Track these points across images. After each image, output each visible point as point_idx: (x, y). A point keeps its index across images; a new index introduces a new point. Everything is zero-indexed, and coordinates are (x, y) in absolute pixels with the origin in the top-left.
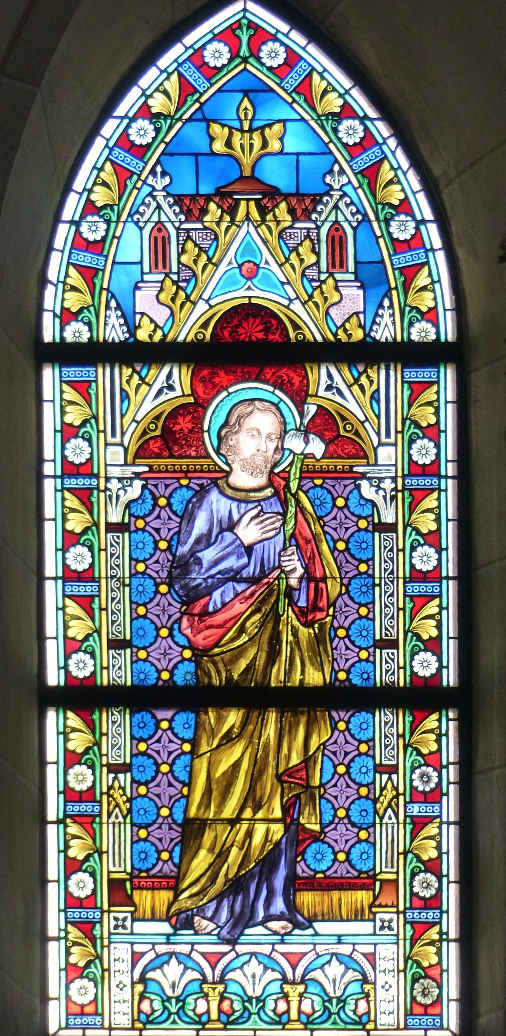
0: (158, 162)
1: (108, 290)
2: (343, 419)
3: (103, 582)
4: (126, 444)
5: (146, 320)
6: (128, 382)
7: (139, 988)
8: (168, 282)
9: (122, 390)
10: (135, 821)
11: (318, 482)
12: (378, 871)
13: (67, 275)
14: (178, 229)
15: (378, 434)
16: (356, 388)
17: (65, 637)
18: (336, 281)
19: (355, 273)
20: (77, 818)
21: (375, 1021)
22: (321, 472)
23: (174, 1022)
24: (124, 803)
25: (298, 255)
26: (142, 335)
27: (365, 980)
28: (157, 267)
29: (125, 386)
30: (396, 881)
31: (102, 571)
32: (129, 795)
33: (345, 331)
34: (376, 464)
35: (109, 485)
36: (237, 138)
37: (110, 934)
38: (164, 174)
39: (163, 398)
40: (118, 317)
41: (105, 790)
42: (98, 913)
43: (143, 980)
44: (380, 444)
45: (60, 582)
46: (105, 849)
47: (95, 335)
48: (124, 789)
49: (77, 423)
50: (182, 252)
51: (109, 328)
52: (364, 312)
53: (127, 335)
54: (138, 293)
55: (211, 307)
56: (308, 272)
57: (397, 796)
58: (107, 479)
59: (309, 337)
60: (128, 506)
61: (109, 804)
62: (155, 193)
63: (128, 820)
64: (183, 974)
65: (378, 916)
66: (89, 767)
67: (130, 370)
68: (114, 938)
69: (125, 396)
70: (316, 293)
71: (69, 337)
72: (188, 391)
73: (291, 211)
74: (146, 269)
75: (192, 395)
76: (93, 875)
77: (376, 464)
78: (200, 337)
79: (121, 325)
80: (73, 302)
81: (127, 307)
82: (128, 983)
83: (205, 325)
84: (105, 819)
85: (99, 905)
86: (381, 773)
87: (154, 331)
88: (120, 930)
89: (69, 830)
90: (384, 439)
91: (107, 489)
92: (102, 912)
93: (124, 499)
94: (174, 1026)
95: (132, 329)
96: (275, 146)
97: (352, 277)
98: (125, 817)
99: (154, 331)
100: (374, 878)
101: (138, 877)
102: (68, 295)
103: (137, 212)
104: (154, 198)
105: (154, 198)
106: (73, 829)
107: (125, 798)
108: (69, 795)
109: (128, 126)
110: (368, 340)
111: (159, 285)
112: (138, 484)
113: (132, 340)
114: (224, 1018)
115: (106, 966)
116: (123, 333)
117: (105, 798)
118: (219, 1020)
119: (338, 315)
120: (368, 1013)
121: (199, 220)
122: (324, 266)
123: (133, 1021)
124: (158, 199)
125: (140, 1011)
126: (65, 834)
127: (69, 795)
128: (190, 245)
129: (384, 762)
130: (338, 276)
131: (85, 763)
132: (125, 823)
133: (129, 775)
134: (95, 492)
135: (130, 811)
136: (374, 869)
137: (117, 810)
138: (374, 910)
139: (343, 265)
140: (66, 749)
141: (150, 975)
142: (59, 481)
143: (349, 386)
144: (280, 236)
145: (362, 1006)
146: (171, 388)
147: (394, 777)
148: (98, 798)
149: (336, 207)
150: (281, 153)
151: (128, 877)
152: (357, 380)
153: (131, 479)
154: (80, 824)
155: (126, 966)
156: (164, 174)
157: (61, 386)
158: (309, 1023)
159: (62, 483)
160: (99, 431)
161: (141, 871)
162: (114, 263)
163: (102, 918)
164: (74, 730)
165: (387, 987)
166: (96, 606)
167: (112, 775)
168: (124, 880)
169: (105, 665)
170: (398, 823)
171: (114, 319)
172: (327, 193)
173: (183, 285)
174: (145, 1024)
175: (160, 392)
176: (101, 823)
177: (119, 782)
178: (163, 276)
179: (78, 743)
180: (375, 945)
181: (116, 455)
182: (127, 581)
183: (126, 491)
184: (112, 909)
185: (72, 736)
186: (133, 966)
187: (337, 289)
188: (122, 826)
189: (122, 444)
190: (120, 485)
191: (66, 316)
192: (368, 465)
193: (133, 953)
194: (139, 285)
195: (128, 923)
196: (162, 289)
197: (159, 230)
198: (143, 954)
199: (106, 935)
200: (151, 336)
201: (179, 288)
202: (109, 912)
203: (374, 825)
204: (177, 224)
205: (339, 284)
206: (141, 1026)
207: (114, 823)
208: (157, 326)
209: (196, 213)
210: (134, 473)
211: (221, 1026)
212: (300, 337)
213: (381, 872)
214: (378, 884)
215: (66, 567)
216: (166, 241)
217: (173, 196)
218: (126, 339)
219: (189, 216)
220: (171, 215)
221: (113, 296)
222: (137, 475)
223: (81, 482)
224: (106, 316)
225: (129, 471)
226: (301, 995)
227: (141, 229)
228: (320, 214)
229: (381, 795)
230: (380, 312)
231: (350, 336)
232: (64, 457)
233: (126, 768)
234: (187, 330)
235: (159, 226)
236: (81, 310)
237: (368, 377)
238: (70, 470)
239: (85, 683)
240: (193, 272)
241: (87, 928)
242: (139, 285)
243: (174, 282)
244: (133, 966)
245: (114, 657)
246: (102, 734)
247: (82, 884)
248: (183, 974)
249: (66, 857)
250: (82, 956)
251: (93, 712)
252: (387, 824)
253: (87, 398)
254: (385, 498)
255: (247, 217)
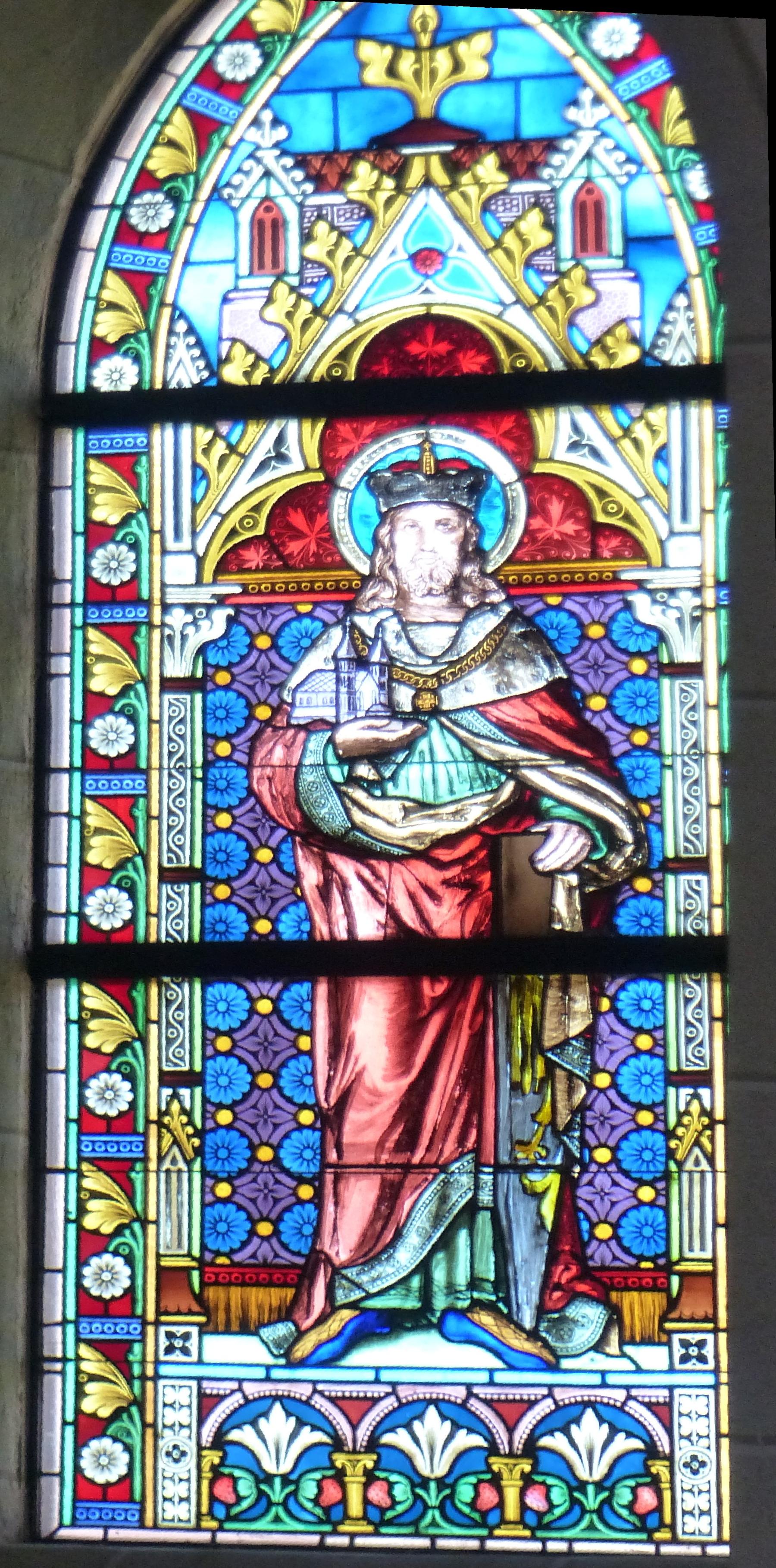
0: (266, 105)
1: (174, 306)
2: (601, 493)
3: (155, 775)
4: (200, 552)
5: (239, 349)
6: (206, 452)
7: (213, 1457)
8: (282, 290)
9: (195, 465)
10: (210, 1166)
11: (554, 600)
12: (675, 1256)
13: (102, 286)
14: (301, 205)
15: (668, 516)
16: (626, 444)
17: (83, 863)
18: (588, 271)
19: (625, 256)
20: (102, 1164)
21: (673, 1527)
22: (560, 583)
23: (277, 1519)
24: (189, 1137)
25: (519, 235)
26: (233, 374)
27: (651, 1451)
28: (261, 266)
29: (201, 459)
30: (712, 1276)
31: (153, 755)
32: (199, 1125)
33: (605, 349)
34: (664, 566)
35: (168, 620)
36: (407, 63)
37: (157, 1362)
38: (276, 122)
39: (268, 475)
40: (189, 347)
41: (154, 1116)
42: (136, 1325)
43: (219, 1442)
44: (672, 533)
45: (77, 776)
46: (152, 1216)
47: (147, 378)
48: (189, 1113)
49: (114, 520)
50: (307, 237)
51: (172, 365)
52: (641, 318)
53: (205, 374)
54: (227, 307)
55: (357, 323)
56: (538, 260)
57: (711, 1126)
58: (166, 608)
59: (538, 361)
60: (202, 650)
61: (160, 1137)
62: (259, 154)
63: (197, 1166)
64: (294, 1436)
65: (676, 1338)
66: (125, 1077)
67: (210, 433)
68: (164, 1370)
69: (200, 474)
70: (553, 293)
71: (103, 382)
72: (315, 463)
73: (505, 166)
74: (244, 269)
75: (322, 468)
76: (129, 1261)
77: (664, 566)
78: (337, 373)
79: (194, 359)
80: (110, 327)
81: (208, 334)
82: (191, 1447)
83: (344, 355)
84: (153, 1166)
85: (139, 1311)
86: (677, 1086)
87: (254, 366)
88: (177, 1356)
89: (87, 1183)
90: (678, 526)
91: (163, 625)
92: (144, 1323)
93: (195, 640)
94: (280, 1527)
95: (214, 366)
96: (476, 69)
97: (620, 263)
98: (189, 1163)
99: (254, 366)
100: (668, 1269)
101: (212, 1264)
102: (102, 317)
103: (228, 184)
104: (259, 161)
105: (259, 161)
106: (95, 1181)
107: (190, 1130)
108: (87, 1121)
109: (216, 52)
110: (649, 362)
111: (266, 293)
112: (221, 615)
113: (213, 383)
114: (374, 1515)
115: (149, 1419)
116: (199, 371)
117: (153, 1128)
118: (365, 1517)
119: (591, 324)
120: (659, 1509)
121: (338, 189)
122: (566, 247)
123: (199, 1516)
124: (265, 161)
125: (213, 1499)
126: (79, 1189)
127: (87, 1121)
128: (321, 228)
129: (684, 1068)
130: (592, 263)
131: (118, 1071)
132: (190, 1171)
133: (198, 1091)
134: (143, 630)
135: (199, 1151)
136: (667, 1254)
137: (175, 1150)
138: (668, 1325)
139: (600, 247)
140: (82, 1047)
141: (234, 1435)
142: (79, 612)
143: (614, 441)
144: (485, 208)
145: (647, 1498)
146: (281, 458)
147: (704, 1092)
148: (141, 1128)
149: (589, 156)
150: (489, 79)
151: (194, 1264)
152: (627, 431)
153: (209, 607)
154: (107, 1173)
155: (187, 1416)
156: (276, 122)
157: (86, 462)
158: (541, 1526)
159: (85, 616)
160: (152, 532)
161: (218, 1253)
162: (187, 263)
163: (143, 1333)
164: (97, 1014)
165: (695, 1465)
166: (140, 814)
167: (167, 1092)
168: (187, 1270)
169: (154, 910)
170: (714, 1171)
171: (182, 351)
172: (570, 135)
173: (306, 291)
174: (221, 1522)
175: (263, 466)
176: (146, 1171)
177: (180, 1102)
178: (272, 280)
179: (102, 1037)
180: (671, 1388)
181: (181, 569)
182: (199, 773)
183: (198, 628)
184: (163, 1318)
185: (93, 1024)
186: (201, 1422)
187: (588, 283)
188: (185, 1176)
189: (193, 551)
190: (189, 618)
191: (99, 348)
192: (649, 566)
193: (201, 1395)
194: (231, 296)
195: (193, 1344)
196: (270, 300)
197: (268, 209)
198: (221, 1398)
199: (150, 1357)
200: (247, 374)
201: (300, 296)
202: (157, 1323)
203: (667, 1176)
204: (299, 199)
205: (594, 276)
206: (214, 1524)
207: (168, 1171)
208: (259, 358)
209: (333, 180)
210: (214, 596)
211: (370, 1529)
212: (521, 363)
213: (682, 1259)
214: (675, 1281)
215: (86, 748)
216: (278, 225)
217: (294, 155)
218: (202, 382)
219: (320, 183)
220: (289, 191)
221: (182, 315)
222: (222, 600)
223: (118, 615)
224: (168, 346)
225: (204, 595)
226: (525, 1477)
227: (234, 210)
228: (557, 168)
229: (679, 1124)
230: (671, 316)
231: (611, 357)
232: (88, 577)
233: (192, 1079)
234: (316, 365)
235: (267, 204)
236: (124, 339)
237: (649, 425)
238: (98, 595)
239: (117, 937)
240: (328, 269)
241: (116, 1353)
242: (231, 296)
243: (292, 289)
244: (201, 1422)
245: (169, 898)
246: (148, 1021)
247: (108, 1276)
248: (294, 1436)
249: (80, 1229)
250: (107, 1398)
251: (133, 987)
252: (690, 1173)
253: (133, 479)
254: (680, 621)
255: (427, 182)
